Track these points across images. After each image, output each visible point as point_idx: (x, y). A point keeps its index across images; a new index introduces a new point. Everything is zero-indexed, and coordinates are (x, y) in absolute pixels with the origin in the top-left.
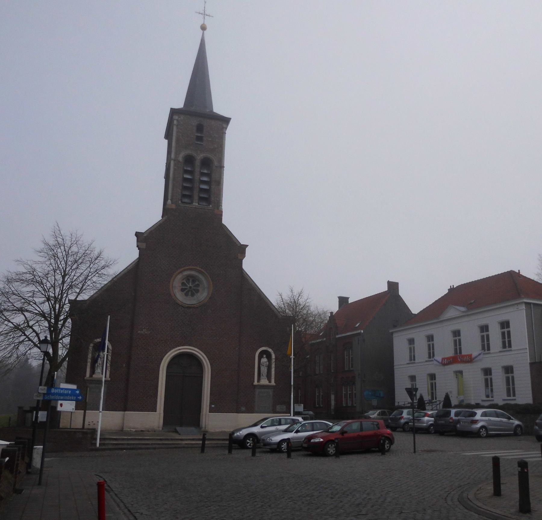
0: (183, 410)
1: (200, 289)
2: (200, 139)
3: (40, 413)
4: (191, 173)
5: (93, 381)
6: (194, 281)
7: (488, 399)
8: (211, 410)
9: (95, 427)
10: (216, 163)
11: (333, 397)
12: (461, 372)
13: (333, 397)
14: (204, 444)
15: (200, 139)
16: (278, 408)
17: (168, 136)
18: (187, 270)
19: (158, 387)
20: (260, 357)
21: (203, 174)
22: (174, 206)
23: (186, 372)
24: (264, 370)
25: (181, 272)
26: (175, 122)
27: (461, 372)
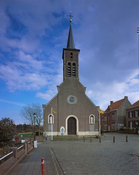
6: (73, 98)
7: (72, 52)
9: (101, 134)
11: (109, 127)
13: (109, 127)
14: (84, 139)
16: (96, 130)
17: (63, 58)
24: (92, 120)
25: (69, 96)
26: (65, 53)
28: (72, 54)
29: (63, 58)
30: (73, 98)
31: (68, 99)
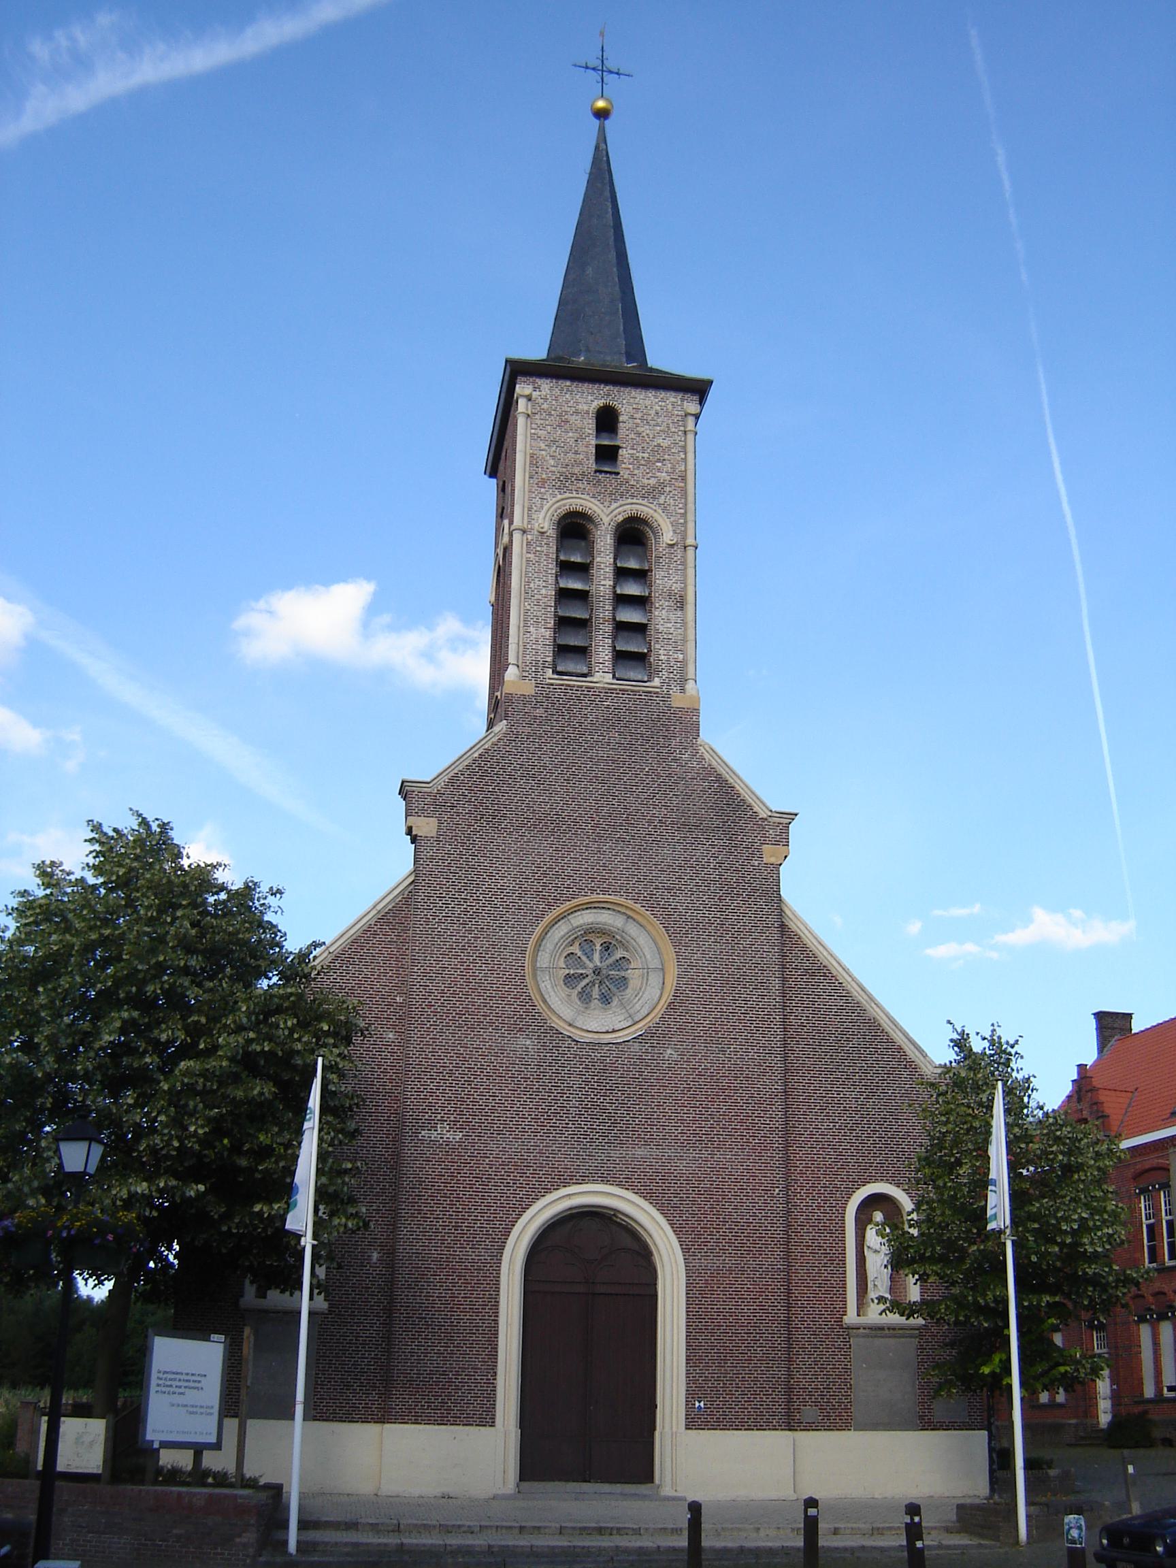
0: (589, 1412)
1: (634, 976)
2: (607, 455)
3: (70, 1427)
5: (266, 1311)
8: (694, 1421)
10: (668, 536)
11: (1103, 1386)
13: (1103, 1386)
16: (939, 1408)
18: (589, 906)
19: (496, 1335)
20: (863, 1220)
22: (528, 688)
23: (592, 1280)
26: (522, 405)
28: (607, 420)
29: (493, 470)
30: (607, 947)
31: (544, 960)
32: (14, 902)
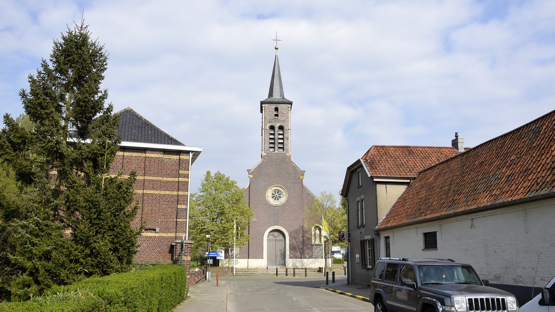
4: (274, 134)
6: (278, 192)
12: (434, 234)
15: (277, 115)
21: (279, 134)
22: (265, 154)
27: (434, 234)
28: (276, 109)
32: (66, 35)
